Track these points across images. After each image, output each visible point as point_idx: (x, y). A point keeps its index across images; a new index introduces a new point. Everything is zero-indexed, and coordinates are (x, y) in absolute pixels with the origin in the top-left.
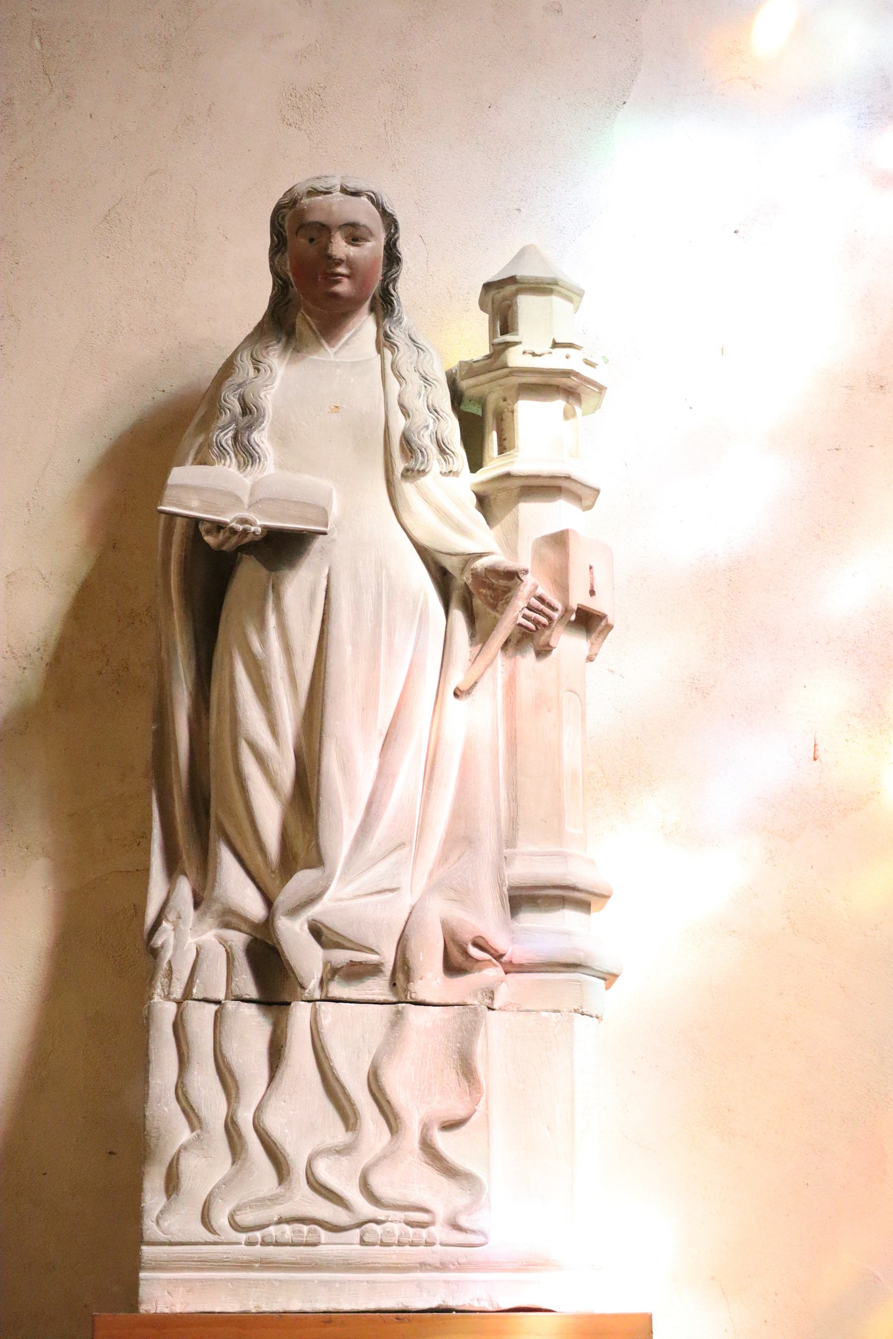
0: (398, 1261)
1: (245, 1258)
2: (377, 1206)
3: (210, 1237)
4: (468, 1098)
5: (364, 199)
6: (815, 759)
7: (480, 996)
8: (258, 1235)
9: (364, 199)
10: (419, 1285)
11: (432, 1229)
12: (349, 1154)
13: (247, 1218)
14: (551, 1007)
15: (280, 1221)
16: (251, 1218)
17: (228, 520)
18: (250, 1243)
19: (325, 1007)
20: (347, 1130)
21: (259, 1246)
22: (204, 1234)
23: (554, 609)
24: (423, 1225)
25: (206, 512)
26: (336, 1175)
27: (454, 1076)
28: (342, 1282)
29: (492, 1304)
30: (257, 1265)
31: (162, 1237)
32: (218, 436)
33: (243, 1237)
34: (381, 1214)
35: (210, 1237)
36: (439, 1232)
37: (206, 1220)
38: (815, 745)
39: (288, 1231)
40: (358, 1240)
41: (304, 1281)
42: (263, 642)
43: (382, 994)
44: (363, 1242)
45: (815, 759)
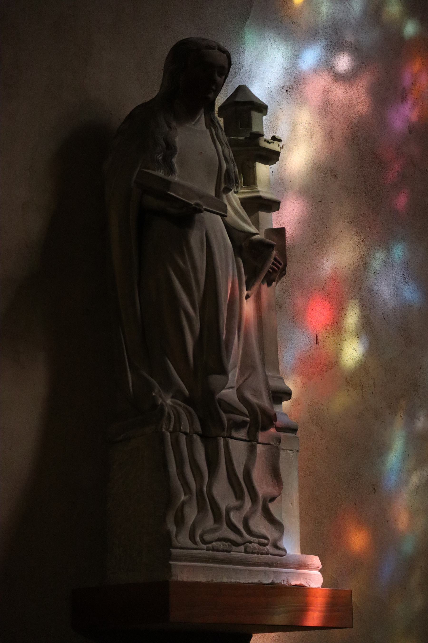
0: (258, 561)
1: (208, 556)
2: (250, 535)
3: (194, 546)
4: (277, 488)
5: (225, 55)
6: (317, 344)
7: (275, 441)
8: (210, 545)
9: (225, 55)
10: (265, 572)
11: (267, 547)
12: (240, 510)
13: (208, 537)
14: (290, 448)
15: (216, 541)
16: (208, 538)
17: (192, 203)
18: (208, 550)
19: (230, 441)
20: (237, 499)
21: (211, 551)
22: (190, 544)
23: (281, 264)
24: (264, 545)
25: (184, 198)
26: (236, 519)
27: (270, 477)
28: (240, 570)
29: (288, 583)
30: (211, 560)
31: (178, 545)
32: (156, 157)
33: (205, 546)
34: (252, 539)
35: (194, 546)
36: (269, 548)
37: (192, 537)
38: (317, 337)
39: (220, 545)
40: (243, 550)
41: (228, 569)
42: (185, 263)
43: (244, 436)
44: (246, 552)
45: (317, 344)
